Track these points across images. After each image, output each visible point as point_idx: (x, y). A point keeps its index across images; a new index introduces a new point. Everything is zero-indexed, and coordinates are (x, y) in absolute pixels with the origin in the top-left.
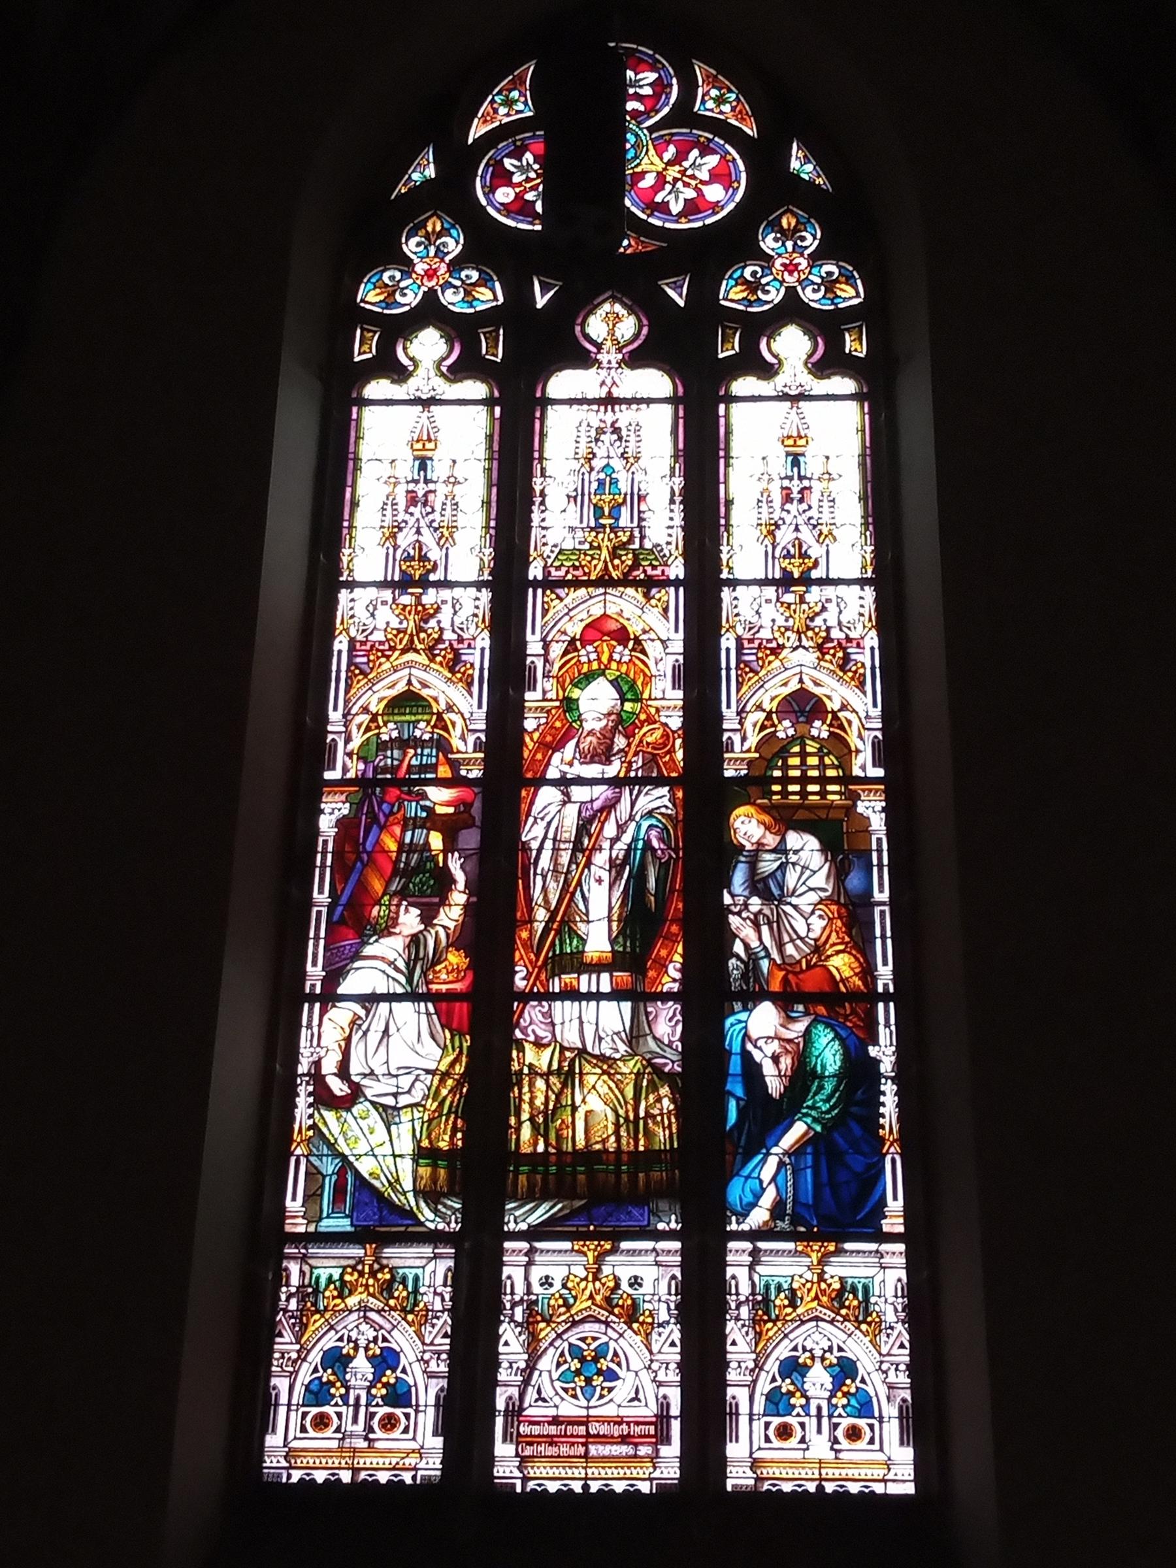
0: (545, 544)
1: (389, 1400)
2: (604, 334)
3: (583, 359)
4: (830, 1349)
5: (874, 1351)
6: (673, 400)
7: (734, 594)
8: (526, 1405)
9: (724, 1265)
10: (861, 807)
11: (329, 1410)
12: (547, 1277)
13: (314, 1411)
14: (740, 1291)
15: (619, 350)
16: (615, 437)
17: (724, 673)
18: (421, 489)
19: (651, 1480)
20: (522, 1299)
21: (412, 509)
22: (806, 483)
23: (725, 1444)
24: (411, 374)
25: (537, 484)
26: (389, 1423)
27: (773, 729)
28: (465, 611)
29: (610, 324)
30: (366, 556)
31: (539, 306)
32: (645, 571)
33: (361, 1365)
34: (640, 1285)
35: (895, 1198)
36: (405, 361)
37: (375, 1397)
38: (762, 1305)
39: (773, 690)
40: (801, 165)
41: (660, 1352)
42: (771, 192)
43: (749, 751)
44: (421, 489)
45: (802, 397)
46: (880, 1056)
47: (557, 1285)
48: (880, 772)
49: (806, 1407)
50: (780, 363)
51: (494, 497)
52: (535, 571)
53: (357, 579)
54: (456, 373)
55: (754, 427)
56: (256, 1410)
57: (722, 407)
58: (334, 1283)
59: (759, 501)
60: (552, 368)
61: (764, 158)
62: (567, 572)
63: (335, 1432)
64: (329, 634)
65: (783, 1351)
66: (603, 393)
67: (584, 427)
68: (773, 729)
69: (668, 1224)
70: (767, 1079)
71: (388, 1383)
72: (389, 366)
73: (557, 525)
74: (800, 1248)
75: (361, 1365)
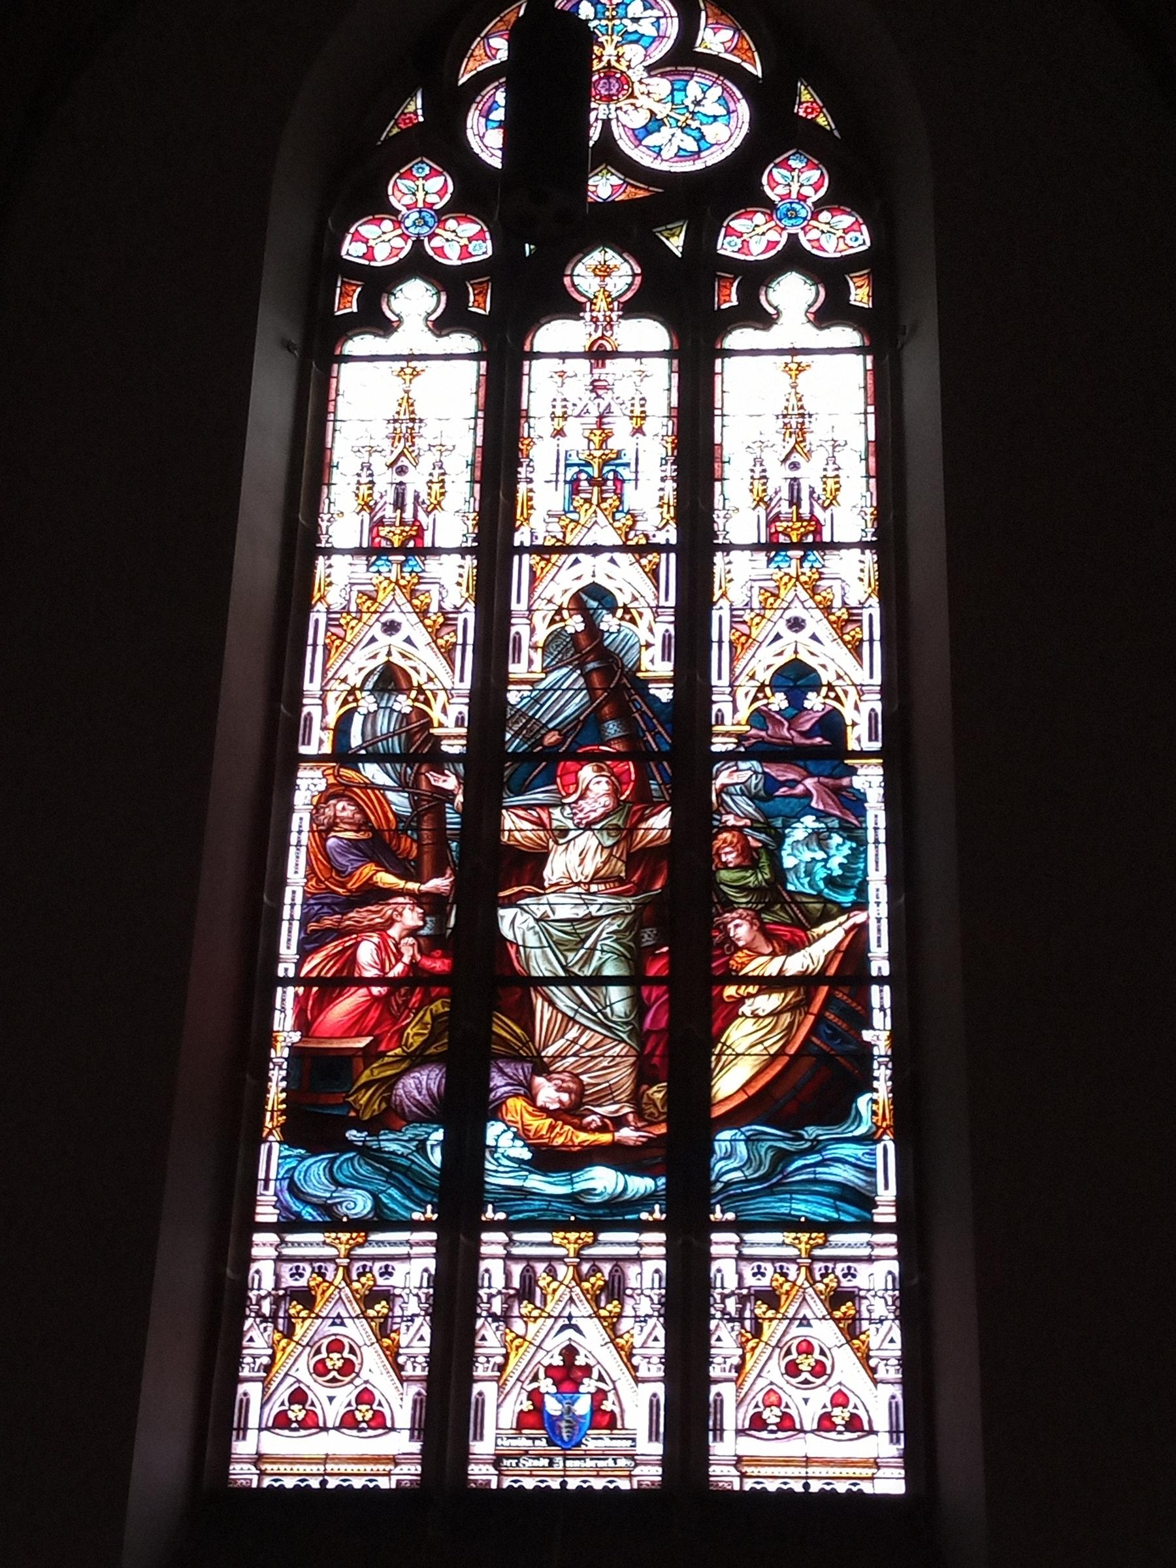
2: (595, 288)
3: (572, 308)
20: (269, 1294)
29: (605, 274)
34: (854, 1276)
35: (886, 1187)
39: (764, 662)
41: (407, 1347)
43: (739, 724)
48: (877, 746)
50: (779, 313)
53: (336, 546)
55: (747, 388)
69: (424, 1213)
72: (756, 315)
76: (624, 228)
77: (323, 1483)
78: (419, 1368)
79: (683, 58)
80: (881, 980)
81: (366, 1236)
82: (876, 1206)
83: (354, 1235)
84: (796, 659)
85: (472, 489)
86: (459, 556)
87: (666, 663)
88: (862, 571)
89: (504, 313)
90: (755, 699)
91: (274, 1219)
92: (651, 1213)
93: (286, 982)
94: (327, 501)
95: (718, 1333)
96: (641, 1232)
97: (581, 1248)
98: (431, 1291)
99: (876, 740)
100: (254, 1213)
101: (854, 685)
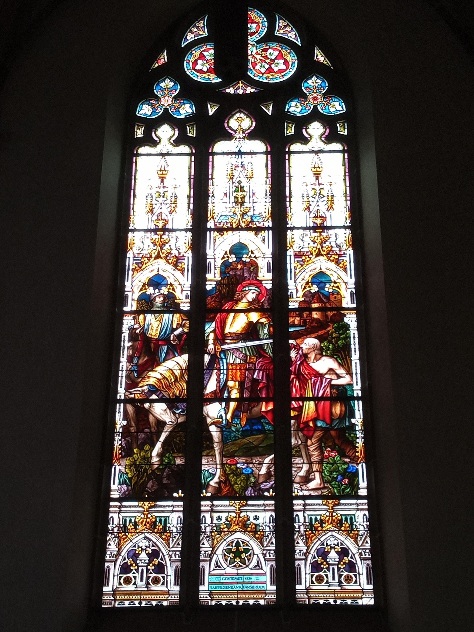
0: (214, 213)
1: (155, 571)
3: (229, 137)
4: (338, 545)
5: (356, 545)
6: (266, 153)
7: (134, 235)
8: (211, 570)
9: (109, 512)
10: (346, 320)
11: (130, 575)
12: (219, 517)
13: (316, 574)
14: (207, 522)
15: (244, 132)
16: (243, 169)
17: (127, 267)
18: (162, 191)
19: (265, 599)
21: (158, 199)
22: (321, 186)
23: (296, 584)
24: (309, 141)
25: (211, 188)
26: (156, 581)
27: (145, 291)
28: (181, 242)
30: (140, 218)
31: (270, 114)
32: (256, 224)
33: (333, 555)
35: (363, 481)
36: (156, 139)
37: (150, 570)
38: (124, 529)
40: (320, 57)
42: (307, 68)
44: (162, 191)
45: (168, 154)
46: (356, 423)
47: (224, 520)
48: (354, 306)
49: (137, 570)
51: (192, 194)
52: (210, 224)
54: (177, 143)
55: (299, 165)
56: (101, 577)
57: (211, 157)
58: (318, 521)
59: (147, 197)
60: (216, 141)
61: (304, 55)
62: (223, 225)
63: (326, 583)
64: (125, 251)
65: (317, 545)
66: (237, 150)
67: (230, 165)
68: (145, 291)
70: (212, 433)
71: (155, 564)
72: (149, 141)
73: (220, 206)
74: (324, 503)
75: (333, 555)
76: (248, 105)
77: (237, 602)
78: (272, 555)
79: (270, 37)
80: (358, 398)
81: (246, 502)
82: (360, 489)
83: (242, 502)
84: (321, 271)
85: (346, 203)
86: (185, 232)
87: (269, 273)
88: (346, 237)
89: (202, 137)
90: (305, 288)
91: (117, 496)
92: (178, 493)
93: (120, 401)
94: (132, 211)
95: (109, 542)
96: (358, 500)
97: (240, 507)
98: (368, 523)
99: (354, 303)
100: (110, 494)
101: (344, 283)
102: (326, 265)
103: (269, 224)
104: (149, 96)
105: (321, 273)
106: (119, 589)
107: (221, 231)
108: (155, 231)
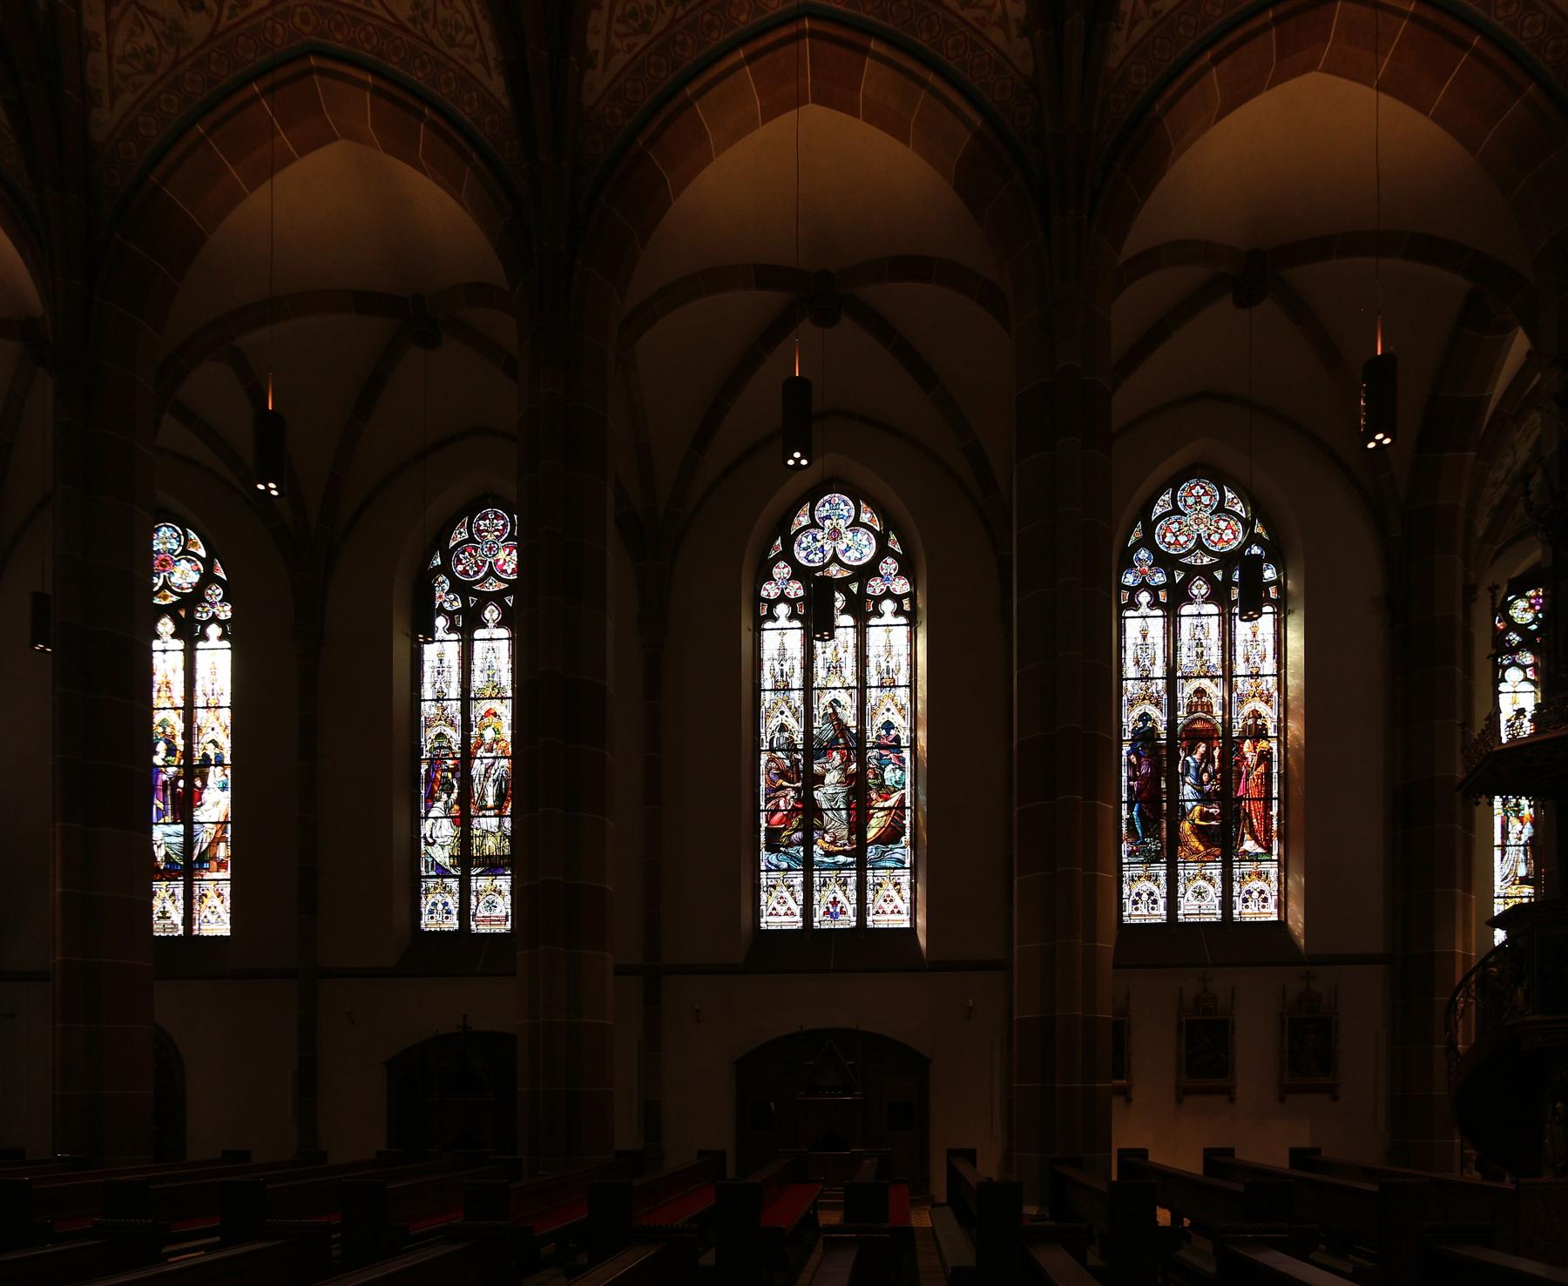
3: (485, 626)
28: (454, 708)
30: (428, 692)
40: (1258, 529)
42: (883, 551)
52: (1179, 674)
55: (875, 637)
61: (881, 539)
72: (1133, 605)
102: (894, 711)
103: (1220, 672)
104: (1128, 564)
105: (1145, 714)
106: (428, 923)
107: (1187, 678)
108: (1251, 676)
